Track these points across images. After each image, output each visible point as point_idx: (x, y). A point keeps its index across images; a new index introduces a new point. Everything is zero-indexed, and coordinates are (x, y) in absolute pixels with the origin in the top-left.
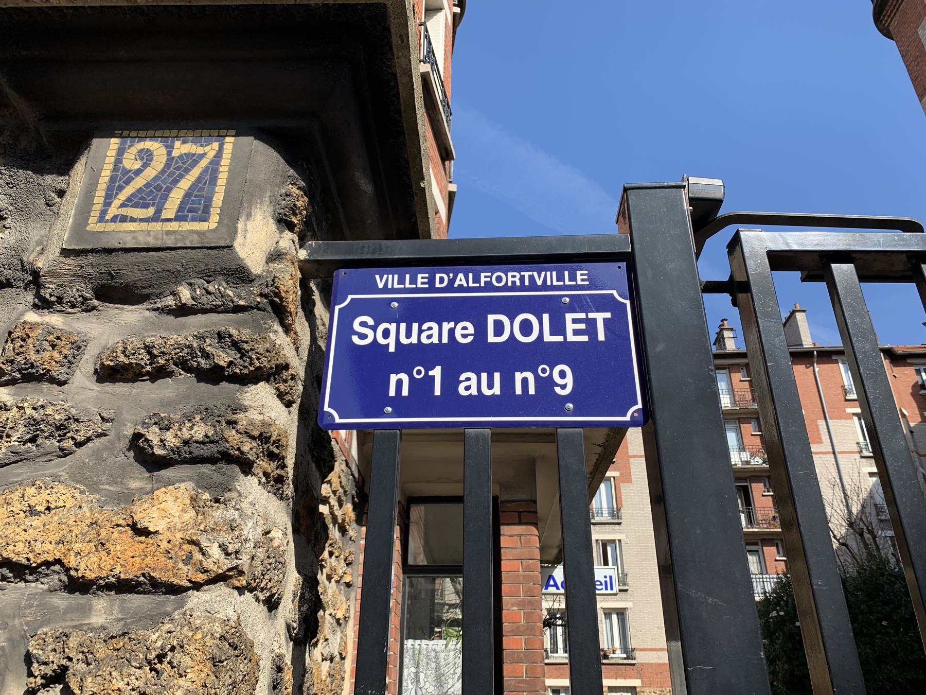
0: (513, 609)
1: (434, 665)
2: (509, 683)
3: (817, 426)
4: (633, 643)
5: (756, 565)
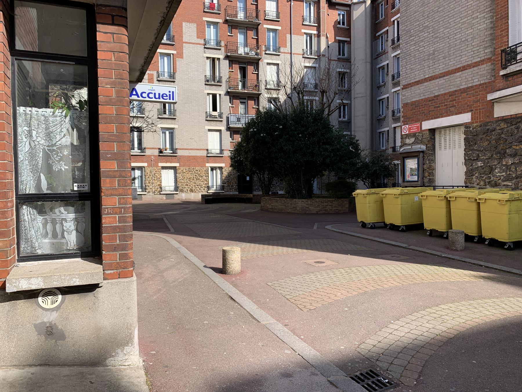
0: (107, 86)
1: (44, 126)
2: (104, 136)
3: (286, 37)
4: (177, 146)
5: (243, 109)
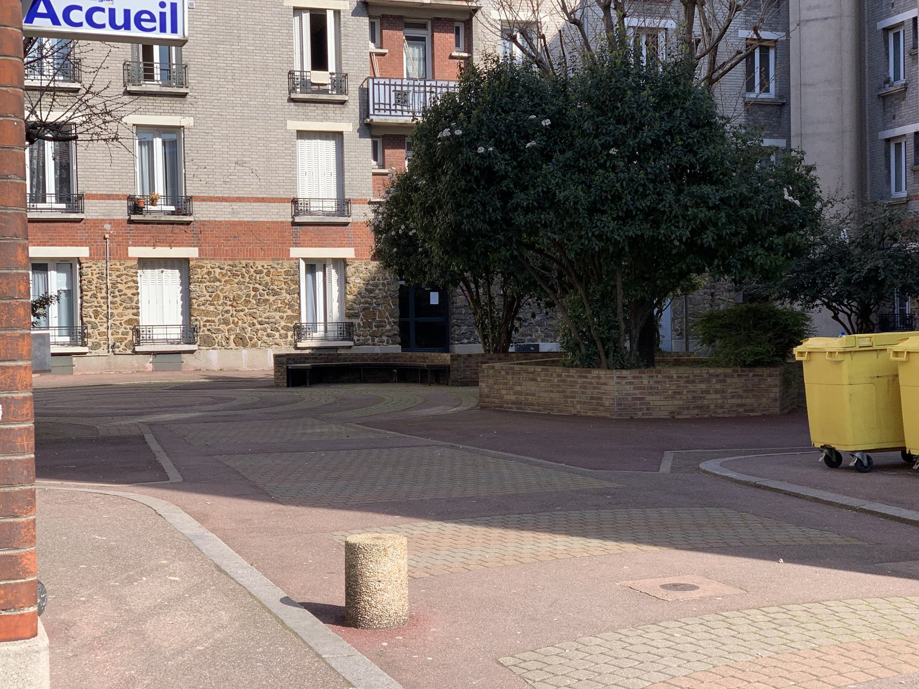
4: (191, 188)
5: (417, 63)
